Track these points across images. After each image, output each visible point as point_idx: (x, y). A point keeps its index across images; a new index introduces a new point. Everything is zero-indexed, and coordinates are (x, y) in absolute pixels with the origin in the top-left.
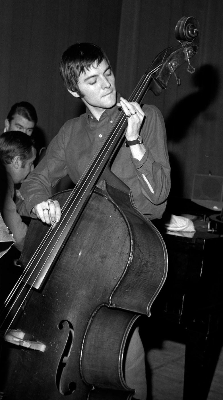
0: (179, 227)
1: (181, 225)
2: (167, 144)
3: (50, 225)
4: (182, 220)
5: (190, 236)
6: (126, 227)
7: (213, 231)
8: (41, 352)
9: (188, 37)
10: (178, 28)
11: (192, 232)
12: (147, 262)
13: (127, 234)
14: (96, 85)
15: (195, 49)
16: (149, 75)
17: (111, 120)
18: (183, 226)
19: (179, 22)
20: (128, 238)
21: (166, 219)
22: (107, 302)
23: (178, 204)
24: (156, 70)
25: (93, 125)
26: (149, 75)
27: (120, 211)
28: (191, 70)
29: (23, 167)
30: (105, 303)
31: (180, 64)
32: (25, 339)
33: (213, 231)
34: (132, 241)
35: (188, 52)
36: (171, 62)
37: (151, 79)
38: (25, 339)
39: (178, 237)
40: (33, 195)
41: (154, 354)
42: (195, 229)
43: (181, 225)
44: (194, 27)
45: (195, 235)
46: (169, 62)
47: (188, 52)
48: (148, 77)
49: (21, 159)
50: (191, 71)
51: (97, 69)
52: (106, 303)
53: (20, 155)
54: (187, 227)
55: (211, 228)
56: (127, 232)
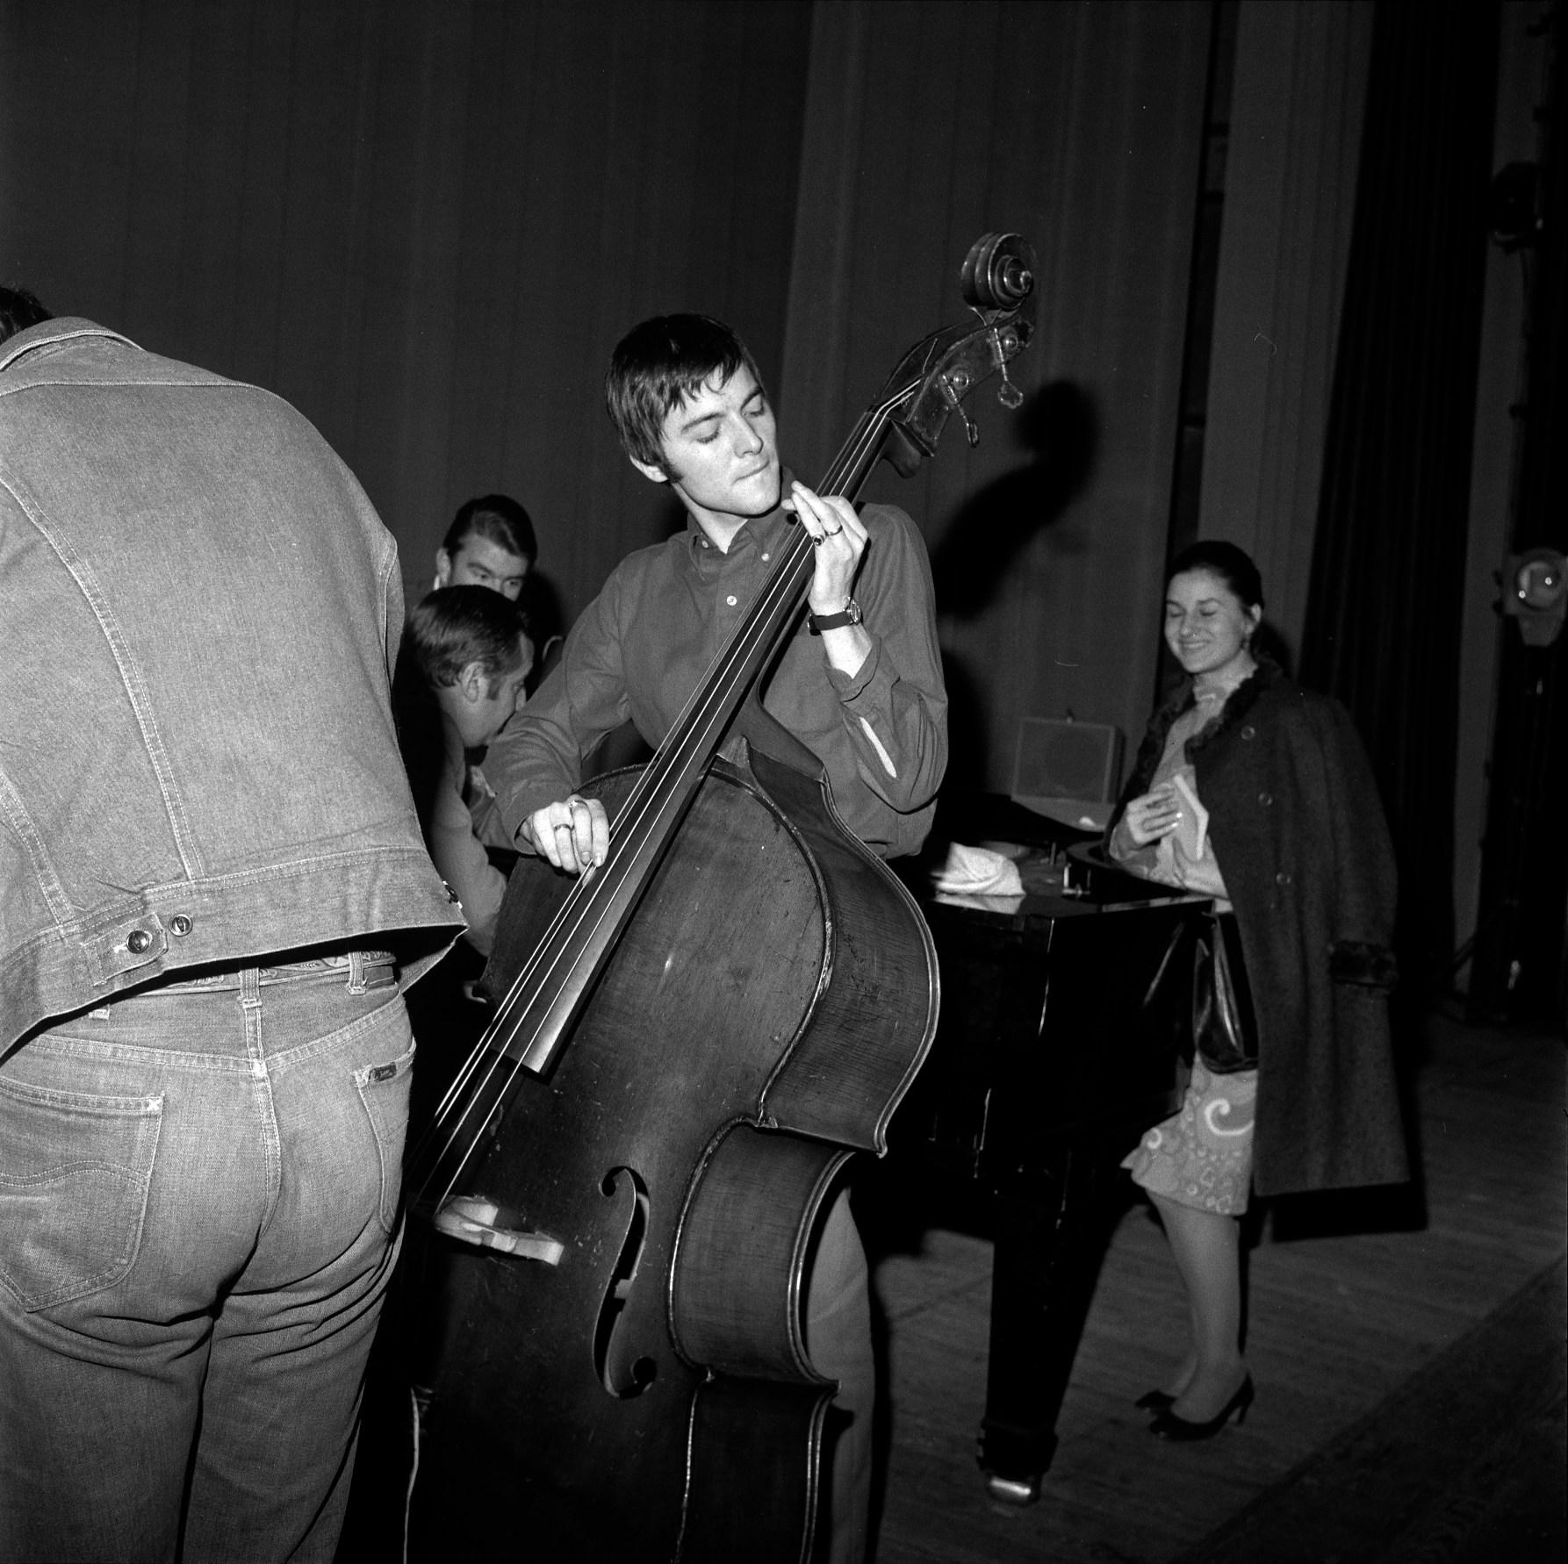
4: (984, 860)
5: (1009, 908)
6: (809, 881)
9: (1002, 295)
11: (1013, 897)
13: (813, 903)
15: (1022, 333)
18: (987, 879)
20: (818, 914)
22: (753, 1112)
23: (969, 810)
25: (707, 568)
28: (1011, 397)
29: (493, 695)
30: (747, 1115)
31: (976, 380)
32: (499, 1225)
34: (828, 924)
35: (1001, 344)
36: (950, 373)
37: (888, 427)
38: (499, 1225)
39: (971, 910)
40: (524, 782)
42: (1024, 887)
44: (1019, 265)
45: (1023, 905)
46: (942, 372)
47: (1001, 344)
48: (879, 418)
49: (486, 671)
50: (1011, 401)
51: (722, 395)
52: (750, 1116)
53: (485, 660)
54: (998, 882)
55: (1072, 885)
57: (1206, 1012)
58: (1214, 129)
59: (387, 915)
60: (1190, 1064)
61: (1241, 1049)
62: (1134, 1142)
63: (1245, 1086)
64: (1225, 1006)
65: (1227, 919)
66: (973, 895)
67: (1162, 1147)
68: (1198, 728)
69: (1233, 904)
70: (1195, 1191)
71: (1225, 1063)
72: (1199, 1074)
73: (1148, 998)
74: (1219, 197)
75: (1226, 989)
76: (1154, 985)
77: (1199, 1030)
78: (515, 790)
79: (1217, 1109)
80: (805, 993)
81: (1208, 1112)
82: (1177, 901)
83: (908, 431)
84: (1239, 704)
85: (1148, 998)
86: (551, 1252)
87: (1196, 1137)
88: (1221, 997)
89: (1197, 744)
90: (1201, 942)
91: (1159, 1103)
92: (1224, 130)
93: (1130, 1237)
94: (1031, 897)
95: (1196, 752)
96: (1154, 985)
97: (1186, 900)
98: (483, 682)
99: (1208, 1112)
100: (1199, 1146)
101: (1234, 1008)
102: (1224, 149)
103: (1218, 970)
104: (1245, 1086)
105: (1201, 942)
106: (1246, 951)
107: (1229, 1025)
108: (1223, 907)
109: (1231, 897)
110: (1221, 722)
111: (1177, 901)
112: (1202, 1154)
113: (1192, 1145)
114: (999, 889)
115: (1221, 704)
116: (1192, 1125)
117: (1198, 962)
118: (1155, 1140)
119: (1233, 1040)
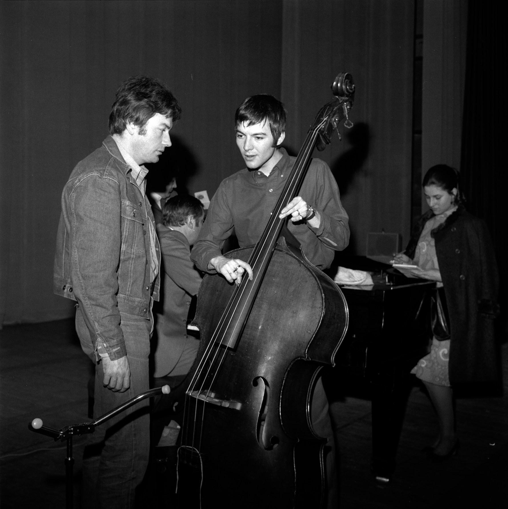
0: (356, 281)
1: (350, 277)
2: (341, 198)
3: (233, 283)
4: (360, 274)
5: (370, 288)
6: (314, 281)
7: (392, 284)
8: (238, 410)
9: (346, 92)
10: (337, 84)
11: (370, 285)
12: (335, 314)
13: (316, 288)
14: (256, 139)
15: (351, 105)
16: (316, 131)
17: (281, 174)
18: (361, 280)
19: (337, 78)
20: (319, 292)
21: (333, 272)
22: (304, 356)
23: (349, 258)
24: (321, 126)
25: (260, 181)
26: (316, 131)
27: (305, 266)
28: (349, 124)
29: (197, 225)
30: (301, 357)
31: (339, 121)
32: (216, 397)
33: (392, 284)
34: (323, 295)
35: (346, 107)
36: (335, 117)
37: (318, 135)
38: (216, 397)
39: (356, 290)
40: (205, 253)
41: (337, 406)
42: (373, 282)
43: (350, 277)
44: (351, 83)
45: (374, 288)
46: (332, 117)
47: (346, 107)
48: (315, 133)
49: (194, 217)
50: (349, 126)
51: (262, 127)
52: (303, 357)
53: (193, 214)
54: (364, 281)
55: (389, 282)
56: (317, 286)
57: (435, 320)
58: (418, 37)
59: (433, 269)
60: (432, 339)
61: (447, 332)
62: (415, 363)
63: (447, 343)
64: (441, 318)
65: (441, 289)
66: (357, 286)
67: (426, 366)
68: (437, 225)
69: (444, 284)
70: (438, 379)
71: (442, 337)
72: (435, 342)
73: (416, 318)
74: (421, 59)
75: (442, 313)
76: (418, 313)
77: (433, 327)
78: (203, 256)
79: (444, 352)
80: (318, 317)
81: (441, 353)
82: (426, 283)
83: (324, 137)
84: (451, 220)
85: (416, 318)
86: (239, 406)
87: (437, 362)
88: (440, 315)
89: (435, 231)
90: (432, 298)
91: (424, 352)
92: (421, 36)
93: (415, 394)
94: (375, 287)
95: (435, 234)
96: (418, 313)
97: (428, 283)
98: (193, 221)
99: (441, 353)
100: (438, 364)
101: (444, 318)
102: (422, 43)
103: (438, 307)
104: (447, 343)
105: (432, 298)
106: (447, 300)
107: (443, 324)
108: (440, 285)
109: (443, 281)
110: (444, 225)
111: (426, 283)
112: (440, 367)
113: (436, 365)
114: (365, 283)
115: (445, 219)
116: (436, 358)
117: (432, 304)
118: (424, 363)
119: (445, 329)
